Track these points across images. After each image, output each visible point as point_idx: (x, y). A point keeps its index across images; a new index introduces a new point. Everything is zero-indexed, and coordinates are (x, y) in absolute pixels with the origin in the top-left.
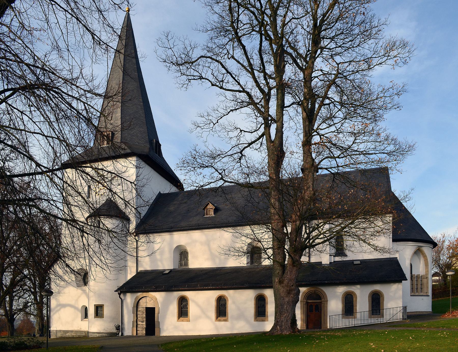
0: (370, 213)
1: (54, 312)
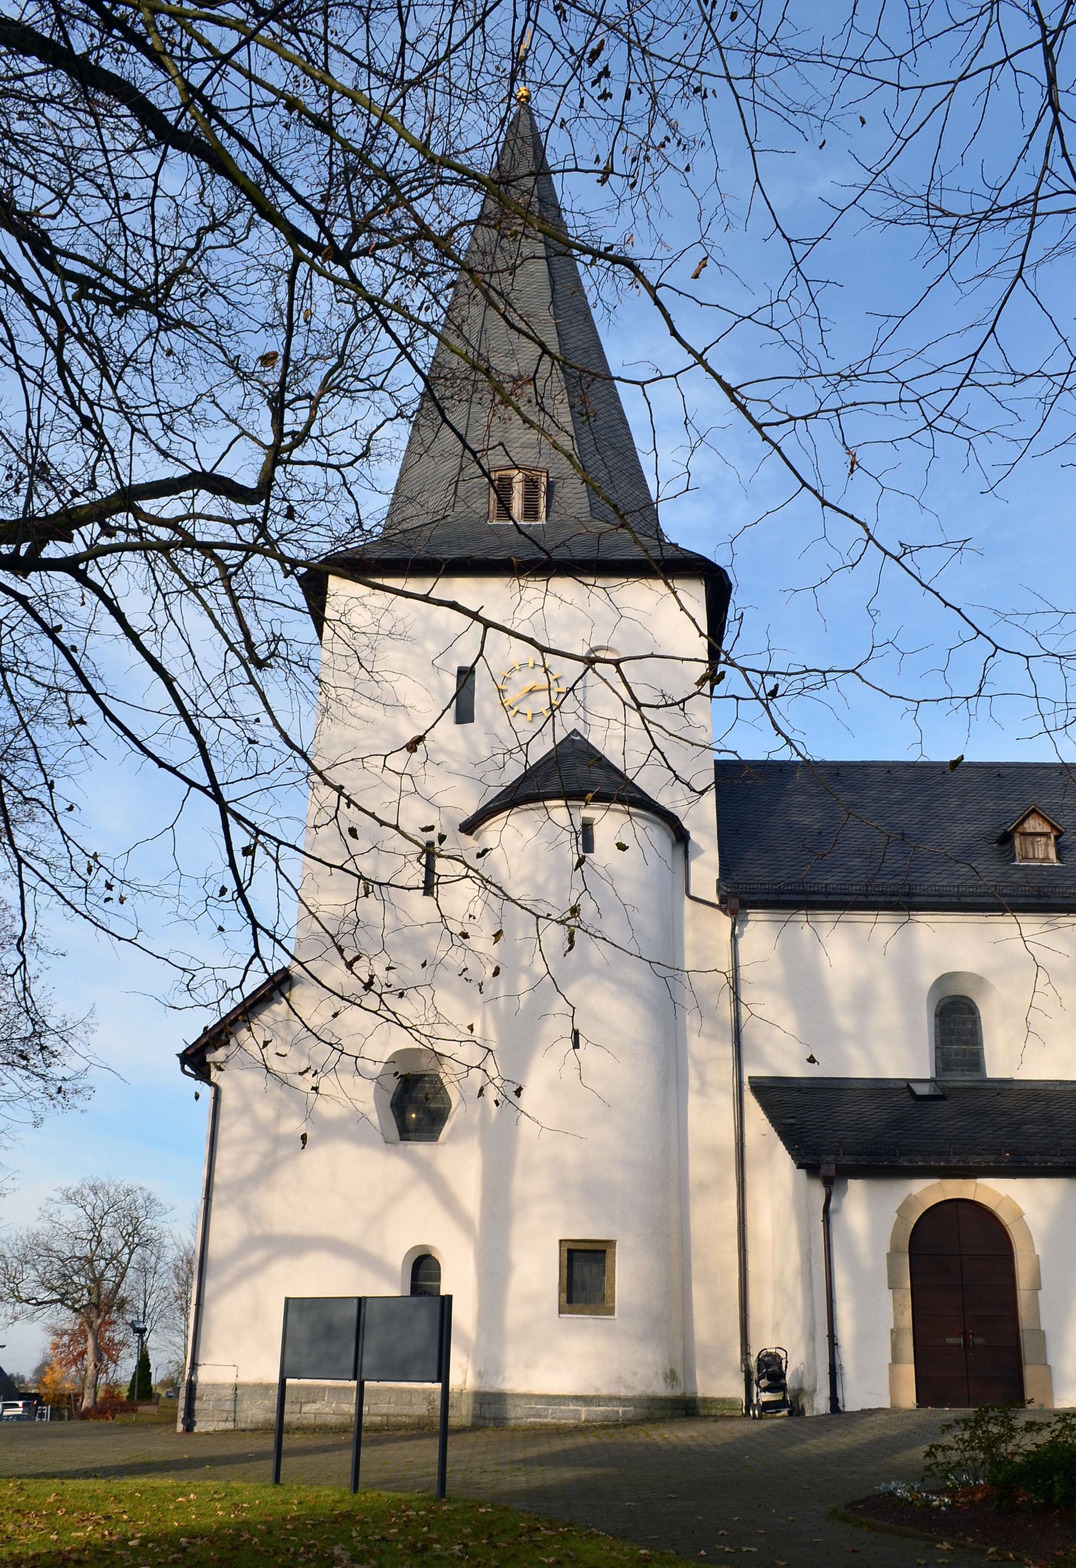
1: (226, 1278)
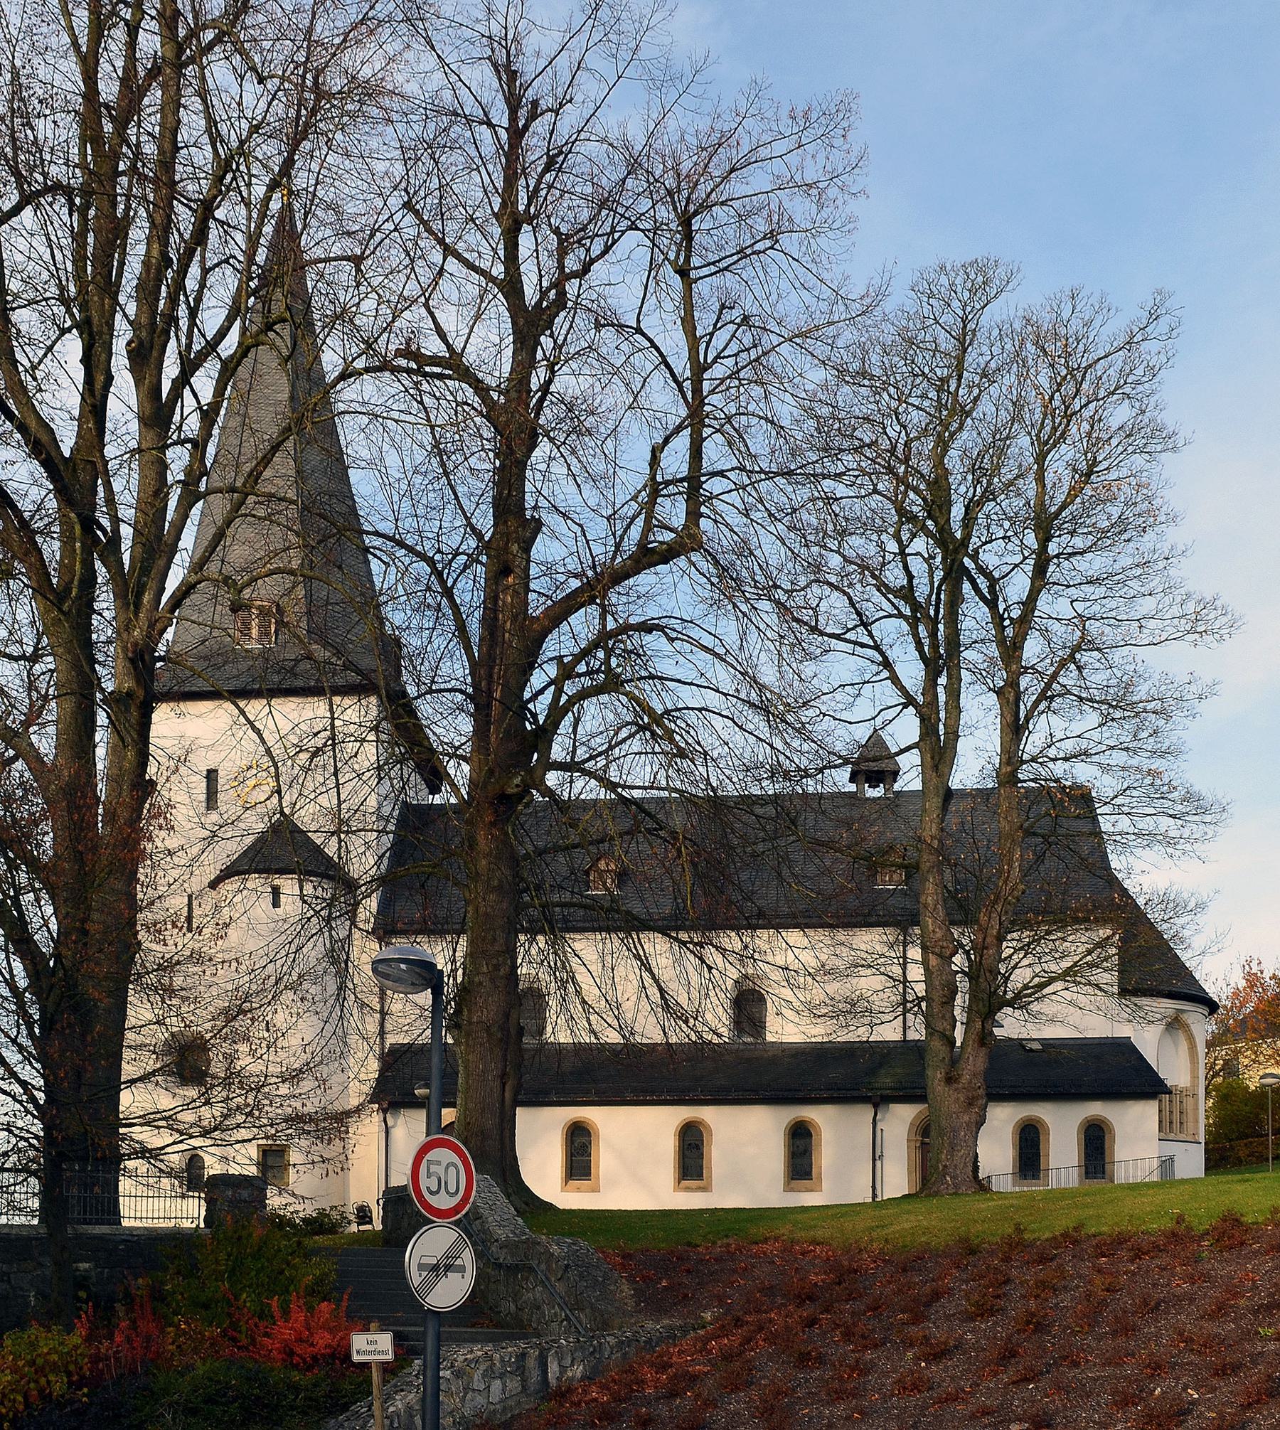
0: (1064, 917)
